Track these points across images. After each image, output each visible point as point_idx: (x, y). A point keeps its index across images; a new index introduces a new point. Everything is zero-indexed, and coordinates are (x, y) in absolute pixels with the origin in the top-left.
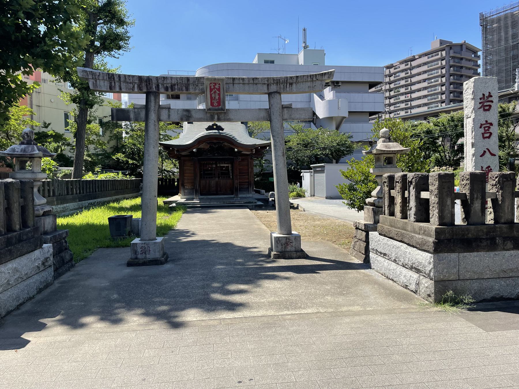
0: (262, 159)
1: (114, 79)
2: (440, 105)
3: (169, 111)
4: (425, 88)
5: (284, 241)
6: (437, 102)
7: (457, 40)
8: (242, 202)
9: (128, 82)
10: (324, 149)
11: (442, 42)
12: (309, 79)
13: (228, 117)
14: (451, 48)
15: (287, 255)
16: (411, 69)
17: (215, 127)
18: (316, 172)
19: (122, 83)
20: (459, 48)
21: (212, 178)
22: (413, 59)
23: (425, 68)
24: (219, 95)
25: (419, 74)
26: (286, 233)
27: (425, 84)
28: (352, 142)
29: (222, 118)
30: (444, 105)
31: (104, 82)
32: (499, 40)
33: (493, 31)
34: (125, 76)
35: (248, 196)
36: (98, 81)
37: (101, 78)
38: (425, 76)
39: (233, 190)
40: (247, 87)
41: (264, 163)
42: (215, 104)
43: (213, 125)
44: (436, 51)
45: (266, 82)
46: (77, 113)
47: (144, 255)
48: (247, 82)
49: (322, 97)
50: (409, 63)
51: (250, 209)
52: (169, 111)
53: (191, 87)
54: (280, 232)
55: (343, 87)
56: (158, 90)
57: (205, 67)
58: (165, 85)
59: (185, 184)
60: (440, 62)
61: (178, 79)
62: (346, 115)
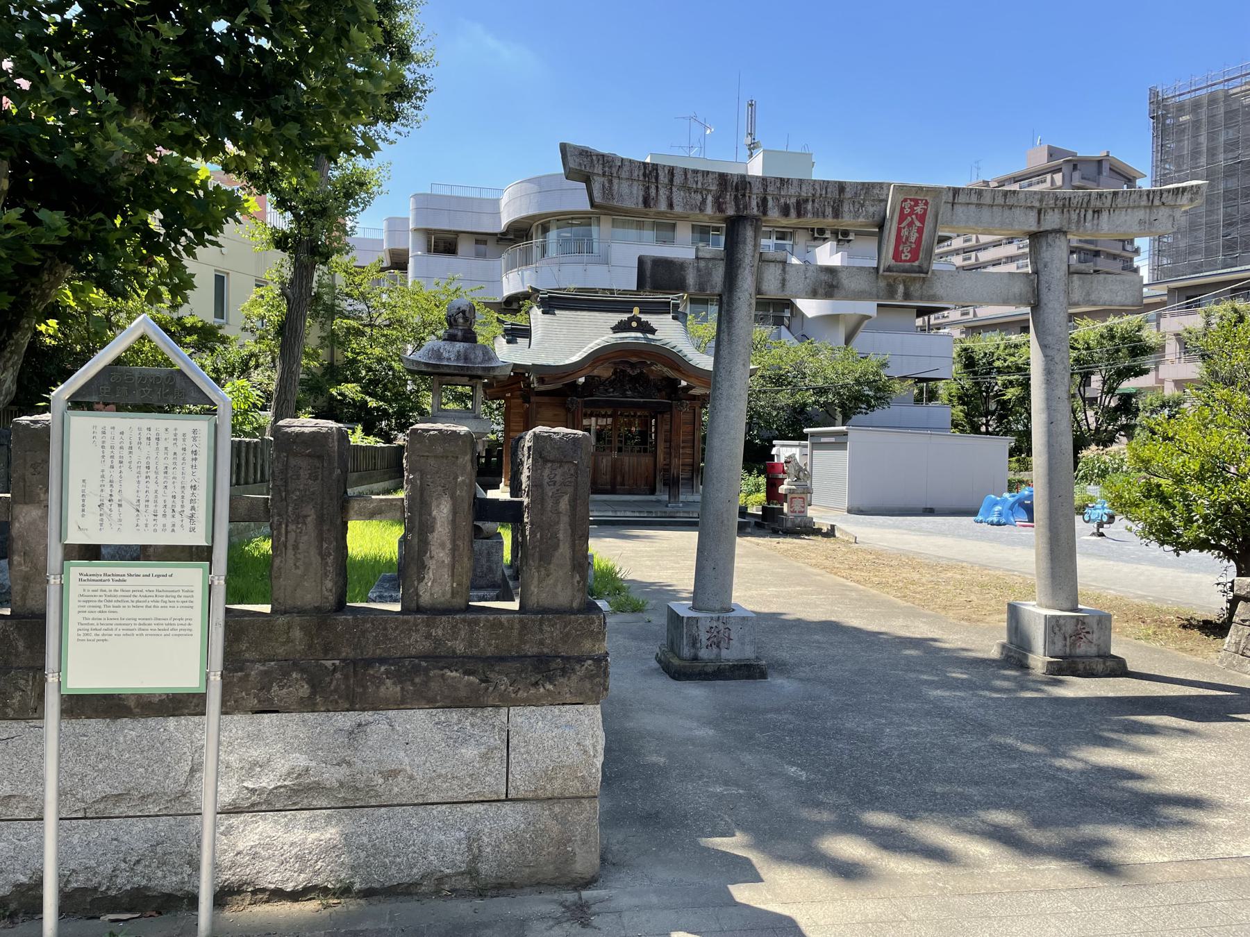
1: (657, 178)
3: (784, 270)
5: (1069, 629)
7: (1088, 150)
9: (689, 189)
10: (821, 391)
12: (1144, 202)
13: (932, 292)
14: (1075, 167)
15: (1081, 666)
17: (634, 324)
18: (815, 446)
19: (674, 189)
20: (1094, 168)
24: (920, 231)
26: (1069, 605)
28: (890, 378)
29: (917, 294)
31: (631, 186)
32: (1195, 154)
33: (1181, 129)
34: (685, 171)
36: (615, 181)
37: (624, 174)
40: (986, 213)
42: (906, 256)
43: (630, 320)
44: (1040, 173)
45: (1037, 204)
46: (288, 273)
47: (715, 650)
48: (987, 200)
52: (784, 270)
53: (846, 208)
54: (1050, 603)
56: (765, 213)
57: (529, 181)
58: (782, 201)
61: (817, 187)
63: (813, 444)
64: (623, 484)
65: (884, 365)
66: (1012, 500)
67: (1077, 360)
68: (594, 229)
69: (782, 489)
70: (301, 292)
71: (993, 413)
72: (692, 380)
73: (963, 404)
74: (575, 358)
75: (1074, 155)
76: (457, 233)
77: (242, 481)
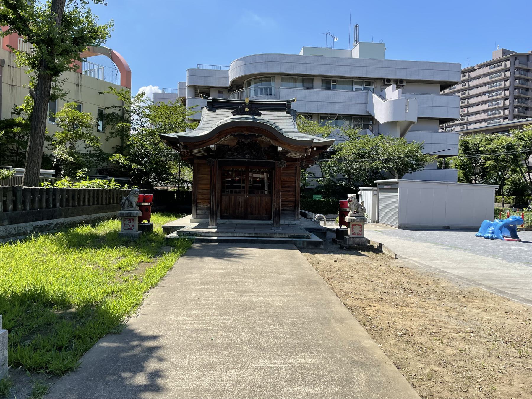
0: (305, 171)
2: (502, 121)
4: (485, 102)
6: (498, 118)
8: (286, 236)
10: (386, 161)
11: (505, 52)
16: (469, 81)
18: (381, 190)
21: (240, 192)
22: (472, 70)
23: (486, 80)
25: (478, 86)
27: (485, 98)
30: (506, 121)
35: (293, 222)
38: (486, 89)
39: (272, 214)
41: (307, 177)
44: (498, 62)
49: (383, 98)
50: (467, 74)
51: (302, 252)
55: (408, 87)
59: (199, 201)
60: (503, 73)
62: (416, 120)
63: (379, 189)
64: (252, 213)
65: (422, 148)
66: (501, 224)
67: (524, 147)
68: (273, 84)
69: (347, 219)
70: (41, 94)
71: (478, 174)
72: (286, 146)
73: (463, 169)
74: (207, 132)
75: (516, 53)
76: (210, 88)
77: (91, 203)
